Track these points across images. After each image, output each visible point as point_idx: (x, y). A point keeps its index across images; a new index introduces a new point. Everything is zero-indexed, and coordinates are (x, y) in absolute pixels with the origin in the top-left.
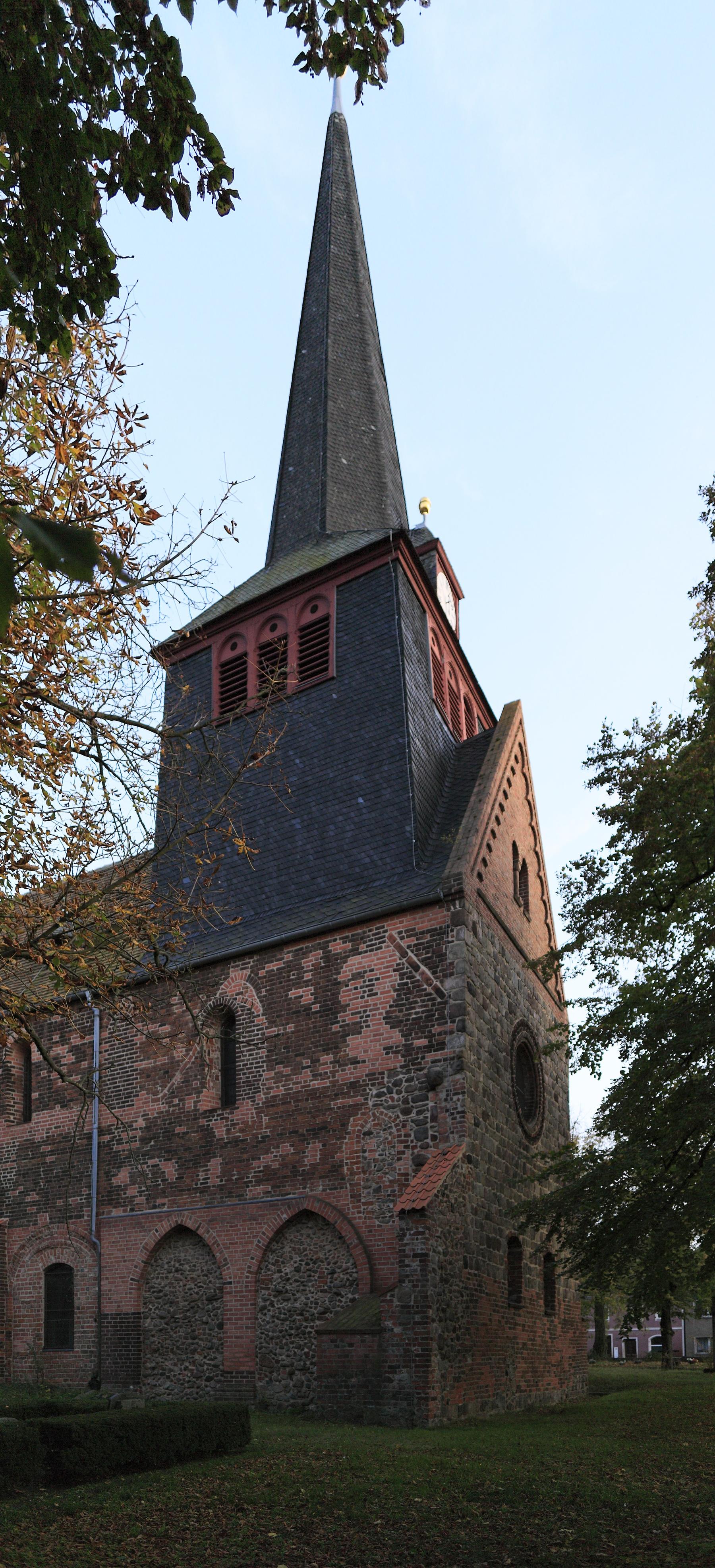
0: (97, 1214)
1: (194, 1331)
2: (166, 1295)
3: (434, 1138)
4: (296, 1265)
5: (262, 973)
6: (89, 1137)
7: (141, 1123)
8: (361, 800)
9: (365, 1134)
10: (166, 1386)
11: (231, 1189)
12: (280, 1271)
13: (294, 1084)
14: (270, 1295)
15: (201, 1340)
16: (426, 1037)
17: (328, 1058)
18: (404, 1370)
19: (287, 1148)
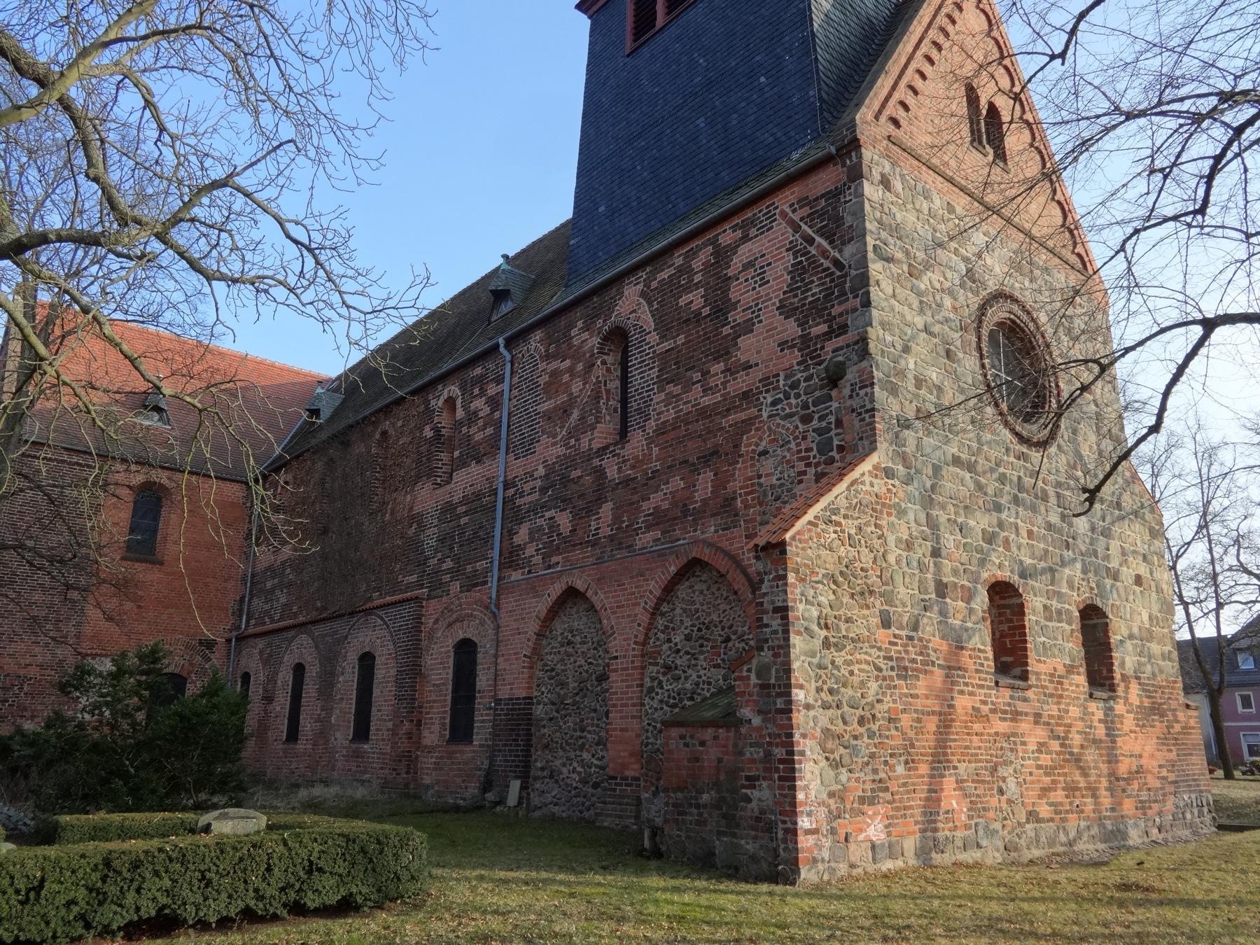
0: (499, 579)
1: (582, 721)
2: (558, 675)
3: (841, 449)
4: (686, 632)
5: (654, 284)
6: (494, 492)
7: (541, 471)
8: (763, 79)
9: (760, 454)
10: (554, 794)
11: (621, 540)
12: (669, 641)
13: (685, 403)
14: (658, 672)
15: (589, 732)
16: (825, 322)
17: (718, 367)
18: (765, 784)
19: (677, 483)
